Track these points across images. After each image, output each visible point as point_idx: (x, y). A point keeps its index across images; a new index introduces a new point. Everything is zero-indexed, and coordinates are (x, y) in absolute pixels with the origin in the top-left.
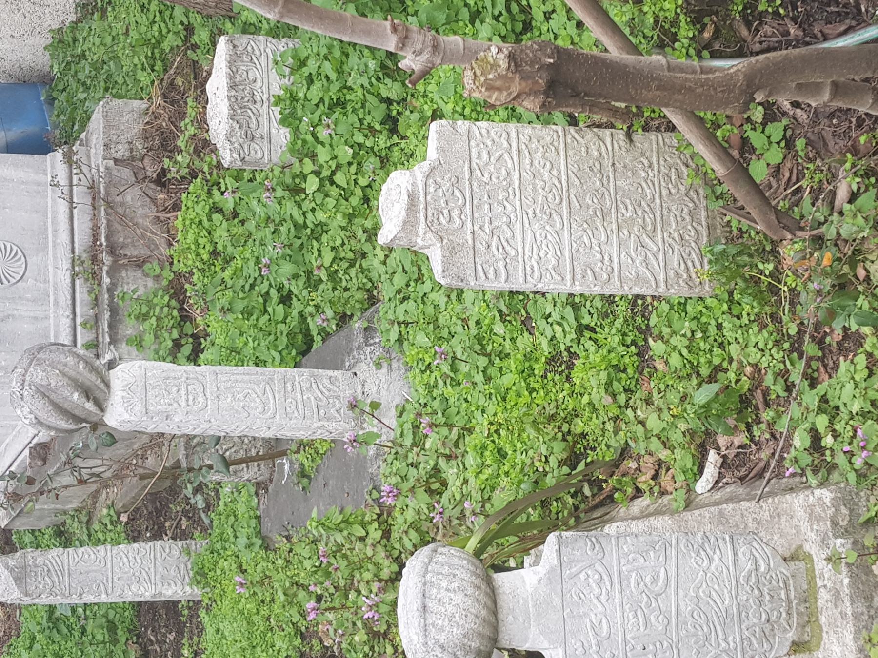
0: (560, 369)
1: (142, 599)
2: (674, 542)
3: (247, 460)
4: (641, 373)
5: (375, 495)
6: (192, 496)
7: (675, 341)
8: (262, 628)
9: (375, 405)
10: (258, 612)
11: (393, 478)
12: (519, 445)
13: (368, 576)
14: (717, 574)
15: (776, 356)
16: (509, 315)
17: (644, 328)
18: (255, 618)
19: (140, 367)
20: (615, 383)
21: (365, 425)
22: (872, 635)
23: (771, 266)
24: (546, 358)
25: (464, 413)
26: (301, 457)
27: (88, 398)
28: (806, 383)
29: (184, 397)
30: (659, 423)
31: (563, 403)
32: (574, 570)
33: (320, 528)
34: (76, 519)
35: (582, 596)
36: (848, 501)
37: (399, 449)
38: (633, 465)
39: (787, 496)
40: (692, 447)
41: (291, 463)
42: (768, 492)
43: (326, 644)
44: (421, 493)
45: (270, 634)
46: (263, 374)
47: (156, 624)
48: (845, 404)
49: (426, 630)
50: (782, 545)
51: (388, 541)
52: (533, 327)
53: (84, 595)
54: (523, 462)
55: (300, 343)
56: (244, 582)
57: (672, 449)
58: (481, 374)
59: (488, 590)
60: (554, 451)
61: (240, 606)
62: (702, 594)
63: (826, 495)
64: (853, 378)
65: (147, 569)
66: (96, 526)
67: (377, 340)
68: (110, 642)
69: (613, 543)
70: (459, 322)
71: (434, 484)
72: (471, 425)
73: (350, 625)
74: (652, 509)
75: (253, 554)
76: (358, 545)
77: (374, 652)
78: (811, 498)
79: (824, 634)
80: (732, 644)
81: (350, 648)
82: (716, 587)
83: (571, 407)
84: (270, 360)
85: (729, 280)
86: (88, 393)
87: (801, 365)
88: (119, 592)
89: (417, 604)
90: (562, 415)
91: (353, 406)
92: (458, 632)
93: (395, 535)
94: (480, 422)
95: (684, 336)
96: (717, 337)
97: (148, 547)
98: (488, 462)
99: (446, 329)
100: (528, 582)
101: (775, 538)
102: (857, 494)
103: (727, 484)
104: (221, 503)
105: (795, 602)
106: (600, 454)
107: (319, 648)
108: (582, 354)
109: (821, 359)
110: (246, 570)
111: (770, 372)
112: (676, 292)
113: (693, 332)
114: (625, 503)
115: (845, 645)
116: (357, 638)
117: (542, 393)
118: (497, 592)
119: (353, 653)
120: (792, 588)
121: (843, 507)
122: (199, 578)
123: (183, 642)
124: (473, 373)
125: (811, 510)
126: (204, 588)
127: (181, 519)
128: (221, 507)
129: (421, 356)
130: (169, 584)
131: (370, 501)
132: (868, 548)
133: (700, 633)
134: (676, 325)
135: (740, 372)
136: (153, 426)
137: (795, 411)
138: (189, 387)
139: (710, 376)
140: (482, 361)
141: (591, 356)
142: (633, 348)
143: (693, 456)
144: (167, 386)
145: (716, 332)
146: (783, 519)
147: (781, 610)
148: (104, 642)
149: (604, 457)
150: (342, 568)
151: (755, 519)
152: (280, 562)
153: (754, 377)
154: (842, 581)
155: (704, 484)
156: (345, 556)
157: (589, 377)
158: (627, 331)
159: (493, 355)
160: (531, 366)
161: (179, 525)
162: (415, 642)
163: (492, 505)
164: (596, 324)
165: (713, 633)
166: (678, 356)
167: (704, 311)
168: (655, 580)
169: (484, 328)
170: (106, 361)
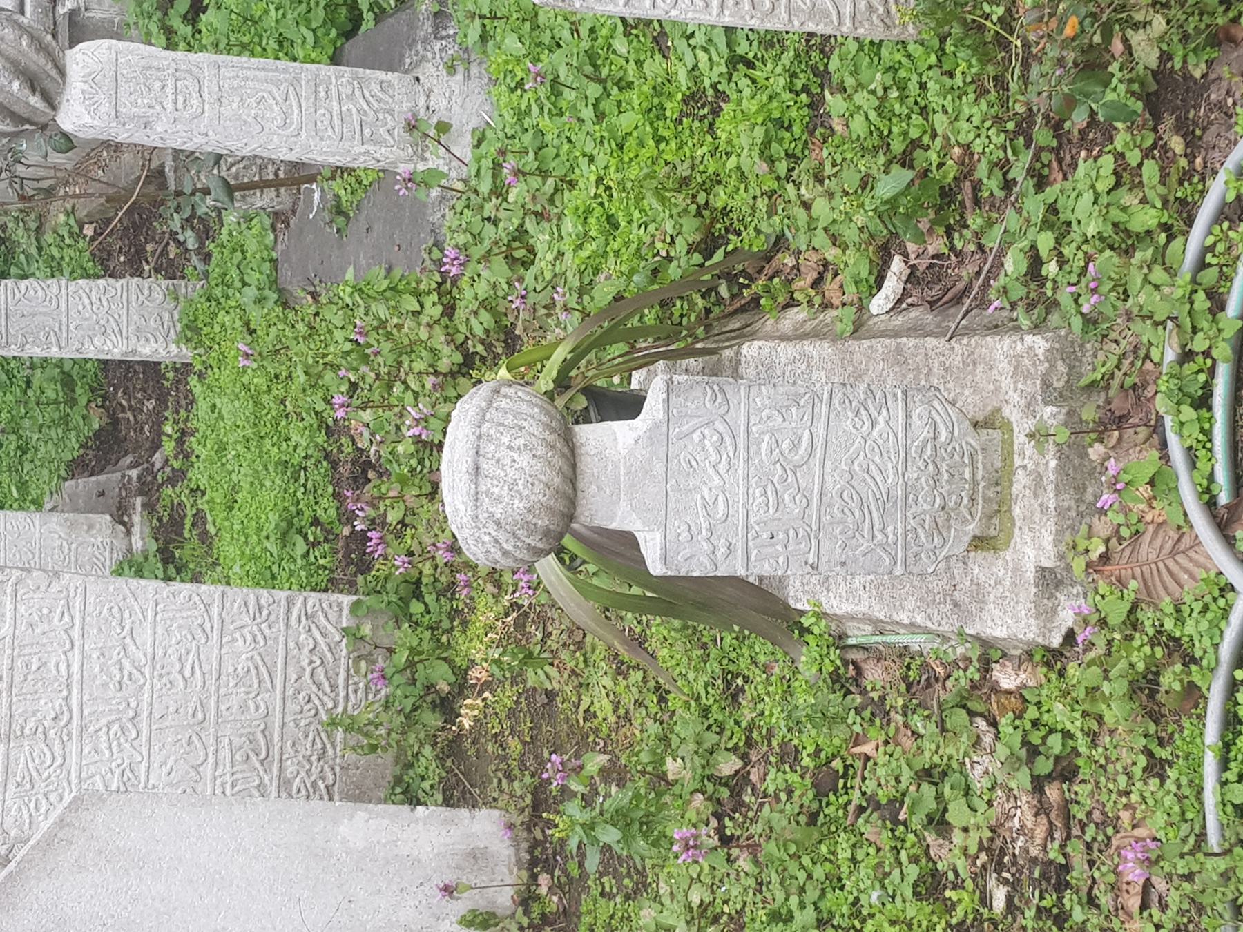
0: (701, 113)
1: (109, 357)
2: (826, 396)
3: (262, 185)
4: (812, 133)
5: (436, 254)
6: (180, 231)
7: (861, 98)
8: (274, 413)
9: (443, 127)
10: (269, 390)
11: (462, 237)
12: (636, 214)
13: (419, 366)
14: (880, 442)
15: (994, 139)
16: (636, 28)
17: (822, 68)
18: (265, 399)
19: (109, 48)
20: (774, 145)
21: (427, 155)
22: (1078, 540)
23: (1000, 11)
24: (683, 95)
25: (565, 158)
26: (337, 186)
27: (34, 91)
28: (1031, 183)
29: (171, 97)
30: (829, 215)
31: (701, 162)
32: (685, 428)
33: (356, 295)
34: (21, 224)
35: (694, 463)
36: (1068, 354)
37: (473, 196)
38: (790, 261)
39: (988, 338)
40: (871, 248)
41: (323, 191)
42: (966, 327)
43: (359, 445)
44: (499, 263)
45: (284, 423)
46: (285, 71)
47: (129, 384)
48: (1079, 222)
49: (477, 500)
50: (973, 404)
51: (450, 320)
52: (668, 48)
53: (28, 346)
54: (640, 240)
55: (343, 19)
56: (250, 352)
57: (844, 248)
58: (591, 107)
59: (566, 450)
60: (684, 229)
61: (245, 380)
62: (857, 469)
63: (1039, 344)
64: (1093, 187)
65: (116, 316)
66: (49, 238)
67: (451, 32)
68: (65, 403)
69: (742, 393)
70: (567, 25)
71: (518, 252)
72: (573, 177)
73: (393, 430)
74: (808, 326)
75: (266, 310)
76: (409, 323)
77: (423, 467)
78: (1019, 344)
79: (1016, 531)
80: (891, 536)
81: (390, 457)
82: (877, 459)
83: (710, 171)
84: (299, 41)
85: (940, 24)
86: (32, 82)
87: (1026, 157)
88: (77, 345)
89: (466, 464)
90: (699, 180)
91: (411, 127)
92: (521, 505)
93: (460, 314)
94: (586, 175)
95: (873, 92)
96: (919, 99)
97: (118, 285)
98: (593, 233)
99: (548, 31)
100: (620, 440)
101: (967, 393)
102: (1081, 346)
103: (912, 305)
104: (224, 231)
105: (982, 484)
106: (746, 240)
107: (350, 450)
108: (734, 96)
109: (1056, 151)
110: (255, 331)
111: (984, 161)
112: (870, 31)
113: (885, 89)
114: (774, 313)
115: (1041, 548)
116: (400, 449)
117: (673, 145)
118: (578, 451)
119: (395, 465)
120: (980, 466)
121: (1060, 363)
122: (189, 334)
123: (166, 414)
124: (580, 105)
125: (1018, 362)
126: (195, 348)
127: (168, 243)
128: (224, 237)
129: (510, 67)
130: (147, 340)
131: (428, 262)
132: (1087, 422)
133: (850, 519)
134: (864, 76)
135: (945, 152)
136: (126, 135)
137: (1012, 220)
138: (179, 83)
139: (904, 152)
140: (594, 90)
141: (744, 101)
142: (803, 96)
143: (871, 261)
144: (147, 79)
145: (918, 91)
146: (980, 368)
147: (963, 494)
148: (56, 402)
149: (750, 246)
150: (385, 352)
151: (942, 364)
152: (302, 328)
153: (964, 161)
154: (1047, 462)
155: (881, 302)
156: (389, 337)
157: (739, 131)
158: (798, 70)
159: (609, 83)
160: (661, 104)
161: (164, 252)
162: (462, 514)
163: (593, 299)
164: (755, 56)
165: (867, 521)
166: (863, 118)
167: (904, 61)
168: (795, 446)
169: (600, 40)
170: (66, 10)
